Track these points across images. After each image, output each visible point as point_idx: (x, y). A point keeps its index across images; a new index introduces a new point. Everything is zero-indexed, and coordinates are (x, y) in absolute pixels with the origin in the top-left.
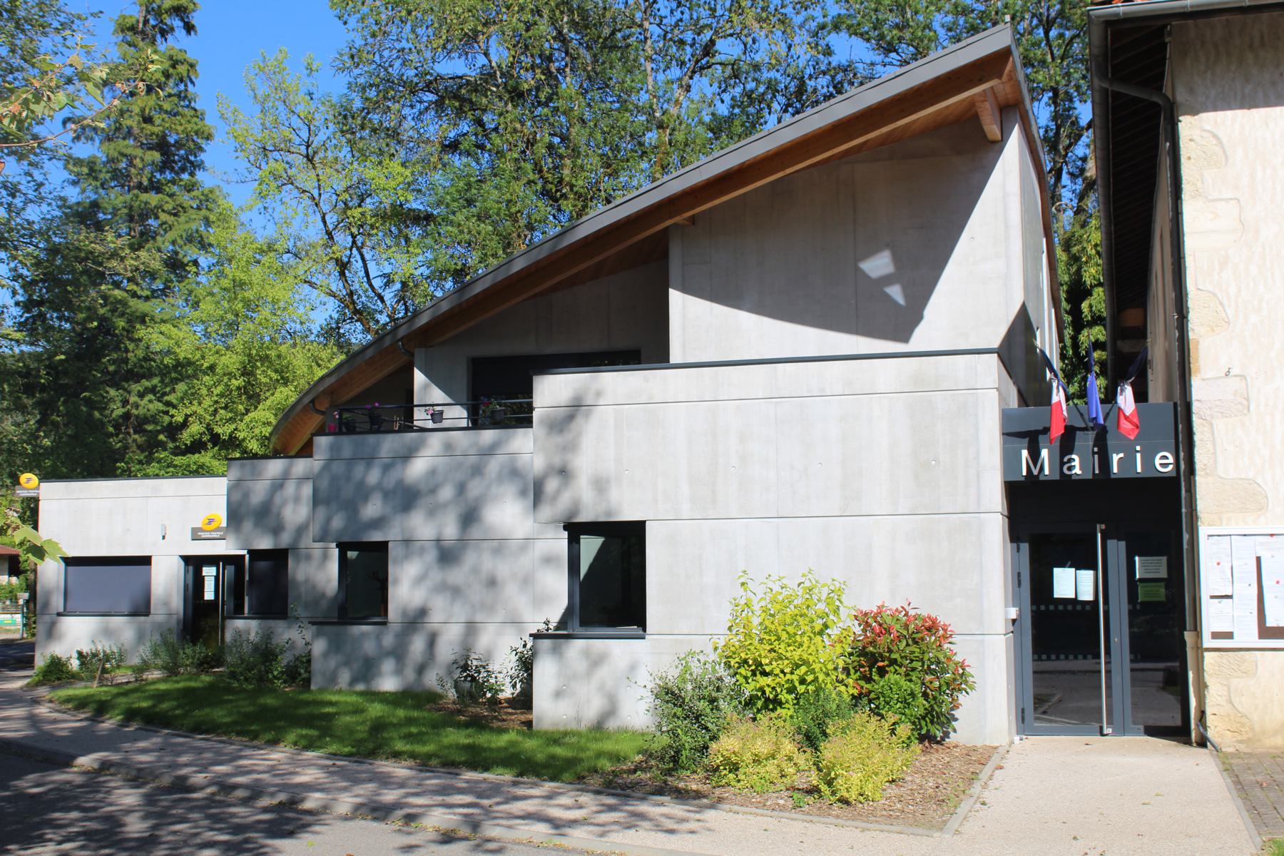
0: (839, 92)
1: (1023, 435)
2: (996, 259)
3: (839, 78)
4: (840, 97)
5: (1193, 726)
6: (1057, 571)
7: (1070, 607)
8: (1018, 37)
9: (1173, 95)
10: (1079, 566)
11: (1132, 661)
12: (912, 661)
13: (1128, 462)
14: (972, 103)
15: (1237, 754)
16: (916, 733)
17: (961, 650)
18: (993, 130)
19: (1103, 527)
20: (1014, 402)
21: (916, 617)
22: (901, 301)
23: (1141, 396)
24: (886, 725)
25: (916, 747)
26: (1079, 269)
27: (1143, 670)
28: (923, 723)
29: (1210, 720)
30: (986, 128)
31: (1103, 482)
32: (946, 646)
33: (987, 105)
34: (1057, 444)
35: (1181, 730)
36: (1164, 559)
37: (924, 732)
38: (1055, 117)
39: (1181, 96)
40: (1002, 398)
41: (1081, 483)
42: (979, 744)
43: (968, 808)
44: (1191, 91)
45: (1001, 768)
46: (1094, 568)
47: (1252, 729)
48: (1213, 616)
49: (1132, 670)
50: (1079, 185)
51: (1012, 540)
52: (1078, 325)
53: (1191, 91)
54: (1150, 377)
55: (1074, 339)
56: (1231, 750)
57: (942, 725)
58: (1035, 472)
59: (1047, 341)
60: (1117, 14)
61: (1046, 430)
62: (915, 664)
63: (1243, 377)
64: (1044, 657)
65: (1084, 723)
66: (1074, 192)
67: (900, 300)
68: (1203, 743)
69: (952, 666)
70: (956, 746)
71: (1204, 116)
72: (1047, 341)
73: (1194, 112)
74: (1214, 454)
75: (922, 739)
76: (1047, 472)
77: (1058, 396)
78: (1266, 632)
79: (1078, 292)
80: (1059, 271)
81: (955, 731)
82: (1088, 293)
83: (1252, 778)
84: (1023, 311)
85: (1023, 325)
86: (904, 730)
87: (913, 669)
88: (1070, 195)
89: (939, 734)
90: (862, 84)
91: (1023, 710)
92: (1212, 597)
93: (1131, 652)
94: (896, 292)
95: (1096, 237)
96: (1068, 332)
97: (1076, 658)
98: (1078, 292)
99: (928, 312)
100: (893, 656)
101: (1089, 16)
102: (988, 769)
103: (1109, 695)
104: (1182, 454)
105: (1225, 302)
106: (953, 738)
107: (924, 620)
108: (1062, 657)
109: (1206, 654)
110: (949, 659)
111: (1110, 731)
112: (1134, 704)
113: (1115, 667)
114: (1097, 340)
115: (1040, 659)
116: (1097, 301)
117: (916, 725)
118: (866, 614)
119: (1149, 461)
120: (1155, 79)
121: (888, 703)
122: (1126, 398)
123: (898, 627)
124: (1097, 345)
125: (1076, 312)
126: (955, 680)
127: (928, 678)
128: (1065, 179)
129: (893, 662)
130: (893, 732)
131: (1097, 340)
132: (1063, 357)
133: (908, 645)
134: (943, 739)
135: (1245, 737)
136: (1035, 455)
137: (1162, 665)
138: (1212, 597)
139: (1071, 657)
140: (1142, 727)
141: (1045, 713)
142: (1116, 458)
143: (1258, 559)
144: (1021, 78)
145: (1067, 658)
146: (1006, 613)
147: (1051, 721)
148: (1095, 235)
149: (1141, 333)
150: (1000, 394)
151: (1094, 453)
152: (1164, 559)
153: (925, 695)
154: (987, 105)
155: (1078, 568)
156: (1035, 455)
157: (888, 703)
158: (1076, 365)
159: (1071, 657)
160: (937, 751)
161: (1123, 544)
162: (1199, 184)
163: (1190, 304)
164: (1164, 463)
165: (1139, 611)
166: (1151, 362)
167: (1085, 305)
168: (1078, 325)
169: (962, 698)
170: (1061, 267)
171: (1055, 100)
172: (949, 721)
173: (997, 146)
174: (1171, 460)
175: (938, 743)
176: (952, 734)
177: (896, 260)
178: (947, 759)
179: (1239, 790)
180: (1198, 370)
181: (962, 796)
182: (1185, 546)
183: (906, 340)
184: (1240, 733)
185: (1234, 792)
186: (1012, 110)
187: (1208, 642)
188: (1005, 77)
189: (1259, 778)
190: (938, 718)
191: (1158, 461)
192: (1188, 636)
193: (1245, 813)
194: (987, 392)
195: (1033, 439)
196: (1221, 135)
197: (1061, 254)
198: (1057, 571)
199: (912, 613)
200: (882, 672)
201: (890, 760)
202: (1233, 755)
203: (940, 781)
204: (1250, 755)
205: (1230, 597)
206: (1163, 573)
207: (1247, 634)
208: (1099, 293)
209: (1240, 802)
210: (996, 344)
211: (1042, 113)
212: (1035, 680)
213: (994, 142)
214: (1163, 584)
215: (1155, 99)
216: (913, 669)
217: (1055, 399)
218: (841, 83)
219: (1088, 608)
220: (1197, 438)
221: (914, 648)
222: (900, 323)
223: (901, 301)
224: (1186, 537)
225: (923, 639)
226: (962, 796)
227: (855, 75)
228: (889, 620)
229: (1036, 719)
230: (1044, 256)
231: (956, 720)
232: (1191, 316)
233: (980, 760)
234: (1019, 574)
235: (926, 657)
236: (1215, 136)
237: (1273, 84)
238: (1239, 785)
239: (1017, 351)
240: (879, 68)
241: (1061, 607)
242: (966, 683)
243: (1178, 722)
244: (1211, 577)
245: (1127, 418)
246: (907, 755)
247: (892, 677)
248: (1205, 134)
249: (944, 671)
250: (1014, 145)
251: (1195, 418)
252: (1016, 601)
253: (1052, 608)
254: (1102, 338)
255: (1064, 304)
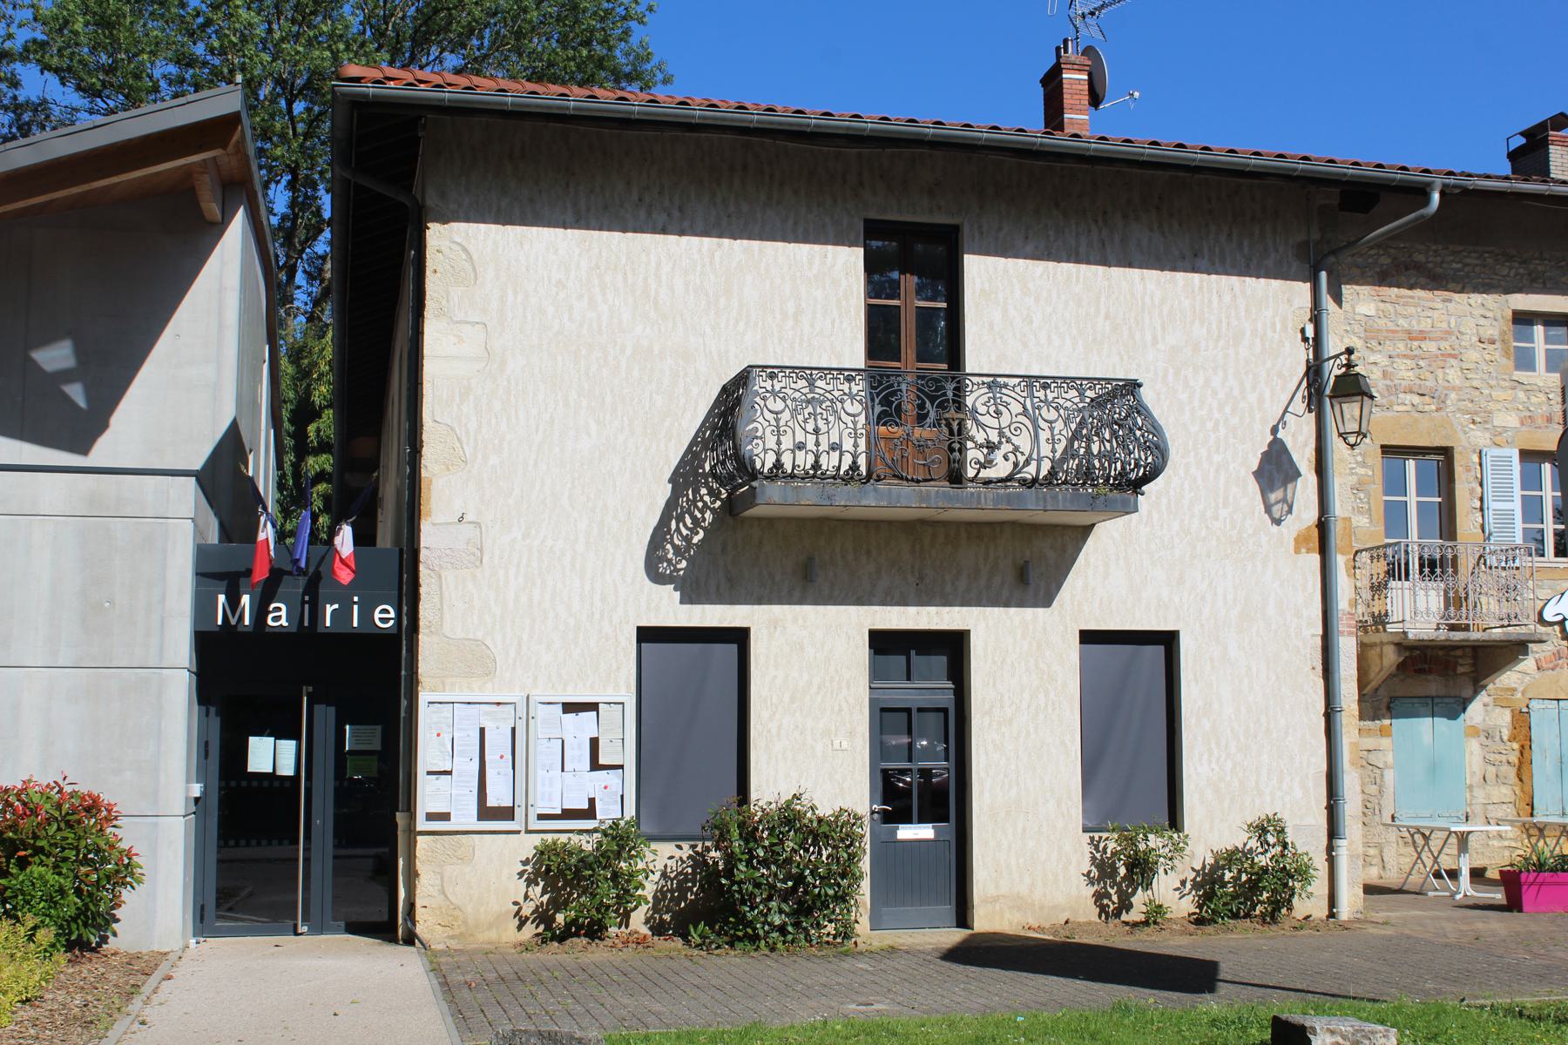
0: (25, 136)
1: (217, 573)
2: (204, 364)
3: (26, 117)
4: (22, 141)
5: (400, 921)
6: (252, 740)
7: (266, 784)
8: (252, 106)
9: (423, 197)
10: (279, 735)
11: (335, 846)
12: (64, 849)
13: (342, 615)
14: (188, 172)
15: (448, 952)
16: (63, 940)
17: (127, 835)
18: (213, 209)
19: (310, 689)
20: (213, 537)
21: (73, 794)
22: (82, 403)
23: (364, 538)
24: (22, 930)
25: (61, 957)
26: (309, 385)
27: (350, 857)
28: (74, 926)
29: (420, 914)
30: (203, 205)
31: (306, 636)
32: (109, 830)
33: (207, 178)
34: (259, 590)
35: (385, 922)
36: (379, 728)
37: (73, 937)
38: (293, 204)
39: (432, 200)
40: (198, 531)
41: (280, 635)
42: (144, 951)
43: (123, 1029)
44: (443, 195)
45: (170, 978)
46: (297, 738)
47: (465, 922)
48: (430, 795)
49: (335, 857)
50: (316, 290)
51: (200, 703)
52: (303, 449)
53: (443, 195)
54: (380, 518)
55: (296, 467)
56: (441, 947)
57: (99, 927)
58: (233, 622)
59: (262, 468)
60: (366, 95)
61: (248, 573)
62: (67, 853)
63: (477, 524)
64: (232, 843)
65: (275, 921)
66: (309, 294)
67: (81, 402)
68: (410, 939)
69: (115, 853)
70: (114, 954)
71: (454, 225)
72: (262, 468)
73: (445, 221)
74: (441, 610)
75: (70, 947)
76: (247, 622)
77: (266, 533)
78: (485, 812)
79: (305, 413)
80: (283, 386)
81: (115, 934)
82: (316, 414)
83: (461, 978)
84: (234, 429)
85: (232, 447)
86: (45, 936)
87: (65, 859)
88: (304, 297)
89: (94, 940)
90: (54, 128)
91: (202, 907)
92: (429, 773)
93: (335, 836)
94: (76, 393)
95: (329, 353)
96: (290, 458)
97: (270, 844)
98: (305, 413)
99: (116, 419)
100: (40, 843)
101: (334, 92)
102: (152, 981)
103: (306, 888)
104: (405, 609)
105: (464, 439)
106: (113, 944)
107: (83, 798)
108: (254, 842)
109: (419, 838)
110: (112, 847)
111: (305, 929)
112: (335, 897)
113: (315, 855)
114: (323, 471)
115: (226, 845)
116: (324, 426)
117: (64, 928)
118: (7, 791)
119: (366, 615)
120: (404, 176)
121: (28, 903)
122: (345, 540)
123: (48, 806)
124: (321, 476)
125: (300, 436)
126: (118, 872)
127: (83, 870)
128: (300, 279)
129: (39, 851)
130: (31, 938)
131: (323, 471)
132: (281, 486)
133: (59, 829)
134: (99, 945)
135: (457, 932)
136: (233, 602)
137: (372, 851)
138: (429, 773)
139: (264, 842)
140: (342, 924)
141: (230, 909)
142: (329, 609)
143: (482, 731)
144: (251, 152)
145: (259, 844)
146: (187, 790)
147: (237, 920)
148: (326, 350)
149: (373, 464)
150: (196, 526)
151: (303, 602)
152: (379, 728)
153: (78, 892)
154: (207, 178)
155: (277, 738)
156: (233, 602)
157: (28, 903)
158: (294, 494)
159: (264, 842)
160: (90, 960)
161: (332, 710)
162: (444, 302)
163: (425, 437)
164: (384, 616)
165: (345, 792)
166: (381, 500)
167: (311, 428)
168: (303, 449)
169: (126, 894)
170: (285, 382)
171: (292, 186)
172: (108, 923)
173: (219, 228)
174: (392, 615)
175: (94, 950)
176: (111, 939)
177: (79, 352)
178: (102, 970)
179: (444, 993)
180: (429, 514)
181: (116, 1015)
182: (403, 714)
183: (84, 450)
184: (451, 927)
185: (439, 995)
186: (238, 189)
187: (422, 824)
188: (230, 148)
189: (468, 978)
190: (94, 919)
191: (377, 615)
192: (400, 818)
193: (449, 1019)
194: (179, 522)
195: (233, 584)
196: (471, 249)
197: (286, 366)
198: (252, 740)
199: (68, 789)
200: (23, 864)
201: (24, 974)
202: (443, 953)
203: (89, 998)
204: (461, 952)
205: (449, 773)
206: (376, 745)
207: (465, 815)
208: (329, 414)
209: (445, 1006)
210: (197, 465)
211: (280, 198)
212: (218, 871)
213: (213, 224)
214: (375, 757)
215: (402, 199)
216: (65, 859)
217: (261, 536)
218: (29, 124)
219: (287, 784)
220: (422, 590)
221: (66, 834)
222: (77, 430)
223: (82, 403)
224: (404, 703)
225: (79, 822)
226: (116, 1015)
227: (48, 117)
228: (36, 798)
229: (219, 917)
230: (266, 367)
231: (118, 921)
232: (425, 451)
233: (144, 967)
234: (207, 743)
235: (83, 843)
236: (465, 250)
237: (531, 201)
238: (446, 987)
239: (222, 479)
240: (83, 115)
241: (255, 784)
242: (132, 875)
243: (385, 918)
244: (429, 751)
245: (342, 560)
246: (48, 966)
247: (36, 870)
248: (454, 247)
249: (105, 861)
250: (238, 227)
251: (421, 568)
252: (202, 775)
253: (244, 784)
254: (328, 468)
255: (286, 425)
